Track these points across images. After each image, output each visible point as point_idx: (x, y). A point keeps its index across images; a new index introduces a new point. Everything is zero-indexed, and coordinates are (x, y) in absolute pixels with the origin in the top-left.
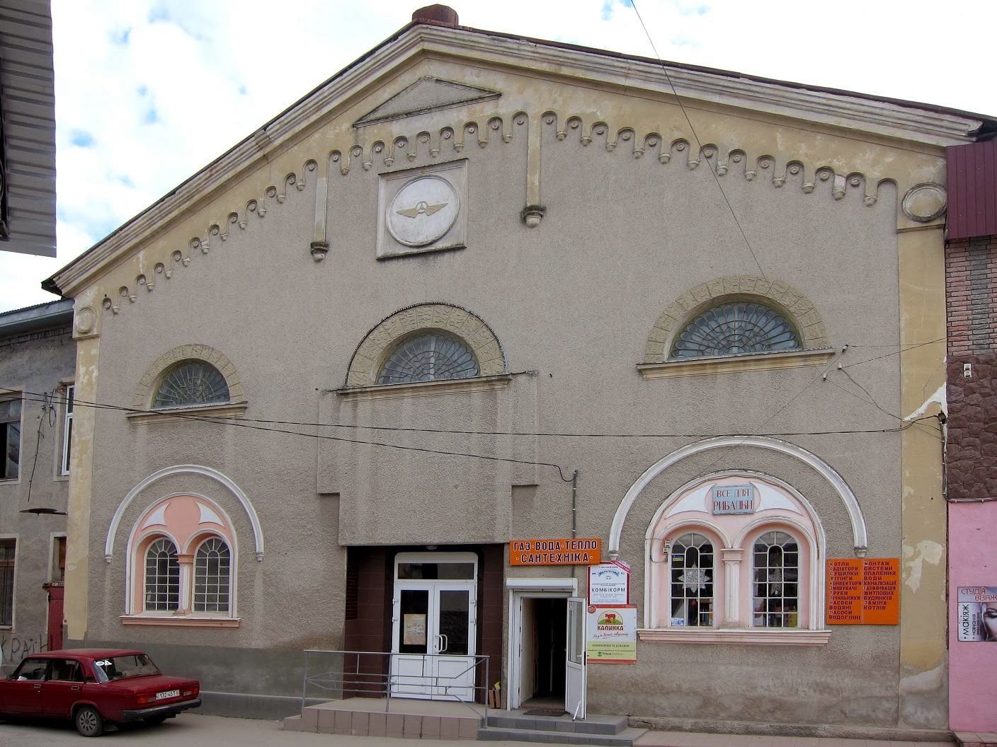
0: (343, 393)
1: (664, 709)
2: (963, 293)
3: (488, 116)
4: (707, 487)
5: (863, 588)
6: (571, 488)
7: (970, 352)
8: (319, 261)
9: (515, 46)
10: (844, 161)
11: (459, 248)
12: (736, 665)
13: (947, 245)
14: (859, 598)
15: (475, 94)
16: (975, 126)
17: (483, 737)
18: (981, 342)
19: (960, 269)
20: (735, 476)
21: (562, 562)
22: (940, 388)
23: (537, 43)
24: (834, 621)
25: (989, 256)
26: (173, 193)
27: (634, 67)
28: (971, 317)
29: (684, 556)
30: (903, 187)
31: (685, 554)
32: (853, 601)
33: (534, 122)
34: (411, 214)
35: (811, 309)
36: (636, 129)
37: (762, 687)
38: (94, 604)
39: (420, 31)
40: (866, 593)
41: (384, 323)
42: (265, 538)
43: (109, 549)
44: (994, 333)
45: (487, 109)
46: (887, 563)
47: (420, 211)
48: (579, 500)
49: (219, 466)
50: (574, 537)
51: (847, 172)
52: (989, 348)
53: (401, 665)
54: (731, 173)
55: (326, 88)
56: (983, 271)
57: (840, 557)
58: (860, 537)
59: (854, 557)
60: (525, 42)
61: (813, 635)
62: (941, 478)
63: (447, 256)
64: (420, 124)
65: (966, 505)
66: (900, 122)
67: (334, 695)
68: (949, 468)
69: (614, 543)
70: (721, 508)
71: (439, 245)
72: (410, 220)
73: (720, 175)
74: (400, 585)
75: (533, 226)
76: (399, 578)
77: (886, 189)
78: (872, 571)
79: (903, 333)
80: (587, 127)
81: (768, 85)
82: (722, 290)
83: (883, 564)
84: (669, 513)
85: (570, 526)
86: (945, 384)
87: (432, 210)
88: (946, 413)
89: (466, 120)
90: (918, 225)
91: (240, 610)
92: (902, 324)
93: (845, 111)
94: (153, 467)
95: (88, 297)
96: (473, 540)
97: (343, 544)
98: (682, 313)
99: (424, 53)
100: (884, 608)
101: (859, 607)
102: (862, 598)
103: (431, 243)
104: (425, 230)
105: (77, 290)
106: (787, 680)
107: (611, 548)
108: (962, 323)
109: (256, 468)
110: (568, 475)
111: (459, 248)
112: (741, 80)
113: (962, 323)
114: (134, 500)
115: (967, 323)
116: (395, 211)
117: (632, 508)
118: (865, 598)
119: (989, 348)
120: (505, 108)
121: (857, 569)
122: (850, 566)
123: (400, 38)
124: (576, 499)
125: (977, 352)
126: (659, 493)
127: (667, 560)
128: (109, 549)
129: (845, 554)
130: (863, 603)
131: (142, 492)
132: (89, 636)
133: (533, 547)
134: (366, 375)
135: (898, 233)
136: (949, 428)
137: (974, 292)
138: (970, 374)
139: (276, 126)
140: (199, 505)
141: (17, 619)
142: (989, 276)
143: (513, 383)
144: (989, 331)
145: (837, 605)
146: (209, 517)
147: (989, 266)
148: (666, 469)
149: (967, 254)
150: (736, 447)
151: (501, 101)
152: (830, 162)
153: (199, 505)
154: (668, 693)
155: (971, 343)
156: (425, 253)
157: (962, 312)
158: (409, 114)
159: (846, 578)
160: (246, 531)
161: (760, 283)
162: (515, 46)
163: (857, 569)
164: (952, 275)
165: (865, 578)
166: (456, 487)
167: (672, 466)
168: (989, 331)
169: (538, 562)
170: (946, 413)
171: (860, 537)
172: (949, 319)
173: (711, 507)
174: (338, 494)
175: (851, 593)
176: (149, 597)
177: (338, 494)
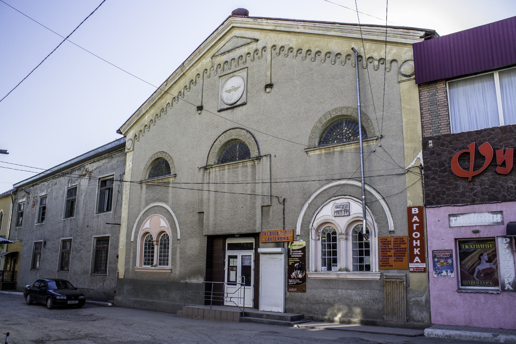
0: (206, 168)
1: (317, 311)
2: (427, 108)
3: (254, 49)
4: (333, 202)
5: (393, 251)
6: (283, 207)
7: (432, 135)
8: (200, 114)
9: (261, 21)
10: (377, 54)
11: (244, 104)
12: (344, 289)
13: (420, 87)
14: (392, 256)
15: (249, 41)
16: (422, 34)
17: (241, 321)
18: (436, 130)
19: (425, 97)
20: (342, 198)
21: (270, 241)
22: (420, 153)
23: (267, 19)
24: (382, 268)
25: (436, 90)
26: (155, 92)
27: (300, 24)
28: (431, 119)
29: (325, 237)
30: (400, 63)
31: (326, 236)
32: (390, 258)
33: (269, 50)
34: (229, 91)
35: (369, 119)
36: (303, 49)
37: (355, 300)
38: (127, 263)
39: (231, 20)
40: (395, 254)
41: (219, 138)
42: (181, 233)
43: (132, 240)
44: (441, 125)
45: (254, 46)
46: (402, 239)
47: (232, 90)
48: (286, 211)
49: (166, 202)
50: (284, 229)
51: (378, 58)
52: (439, 132)
53: (228, 289)
54: (337, 63)
55: (202, 45)
56: (435, 97)
57: (384, 235)
58: (391, 227)
59: (389, 236)
60: (264, 19)
61: (374, 274)
62: (422, 196)
63: (240, 108)
64: (232, 55)
65: (433, 209)
66: (395, 35)
67: (202, 304)
68: (425, 190)
69: (298, 232)
70: (338, 214)
71: (238, 103)
72: (229, 94)
73: (333, 64)
74: (228, 253)
75: (269, 92)
76: (228, 250)
77: (394, 64)
78: (397, 243)
79: (404, 128)
80: (286, 49)
81: (346, 26)
82: (335, 113)
83: (401, 239)
84: (317, 217)
85: (282, 224)
86: (422, 151)
87: (235, 89)
88: (423, 165)
89: (247, 52)
90: (406, 78)
91: (172, 265)
92: (404, 124)
93: (375, 33)
94: (147, 204)
95: (130, 135)
96: (248, 231)
97: (205, 234)
98: (321, 125)
99: (233, 27)
100: (402, 261)
101: (391, 260)
102: (393, 256)
103: (236, 102)
104: (233, 98)
105: (127, 132)
106: (365, 297)
107: (297, 234)
108: (427, 122)
109: (178, 202)
110: (281, 200)
111: (244, 104)
112: (336, 25)
113: (427, 122)
114: (141, 218)
115: (429, 121)
116: (224, 90)
117: (305, 215)
118: (394, 256)
119: (439, 132)
120: (259, 46)
121: (390, 242)
122: (388, 240)
123: (225, 23)
124: (285, 211)
125: (435, 135)
126: (315, 208)
127: (319, 239)
128: (132, 240)
129: (386, 235)
130: (393, 258)
131: (143, 214)
132: (126, 276)
133: (269, 234)
134: (213, 160)
135: (399, 83)
136: (424, 171)
137: (432, 107)
138: (432, 145)
139: (187, 62)
140: (160, 219)
141: (108, 270)
142: (437, 99)
143: (261, 160)
144: (439, 124)
145: (383, 260)
146: (164, 224)
147: (437, 94)
148: (317, 196)
149: (428, 90)
150: (344, 185)
151: (259, 43)
152: (372, 55)
153: (160, 219)
154: (319, 303)
155: (431, 131)
156: (233, 107)
157: (427, 115)
158: (228, 52)
159: (386, 246)
160: (381, 220)
161: (349, 109)
162: (261, 21)
163: (390, 242)
164: (423, 100)
165: (394, 246)
166: (242, 207)
167: (319, 194)
168: (439, 124)
169: (271, 241)
170: (423, 165)
171: (391, 227)
172: (422, 120)
173: (333, 213)
174: (203, 212)
175: (389, 254)
176: (145, 259)
177: (203, 212)
